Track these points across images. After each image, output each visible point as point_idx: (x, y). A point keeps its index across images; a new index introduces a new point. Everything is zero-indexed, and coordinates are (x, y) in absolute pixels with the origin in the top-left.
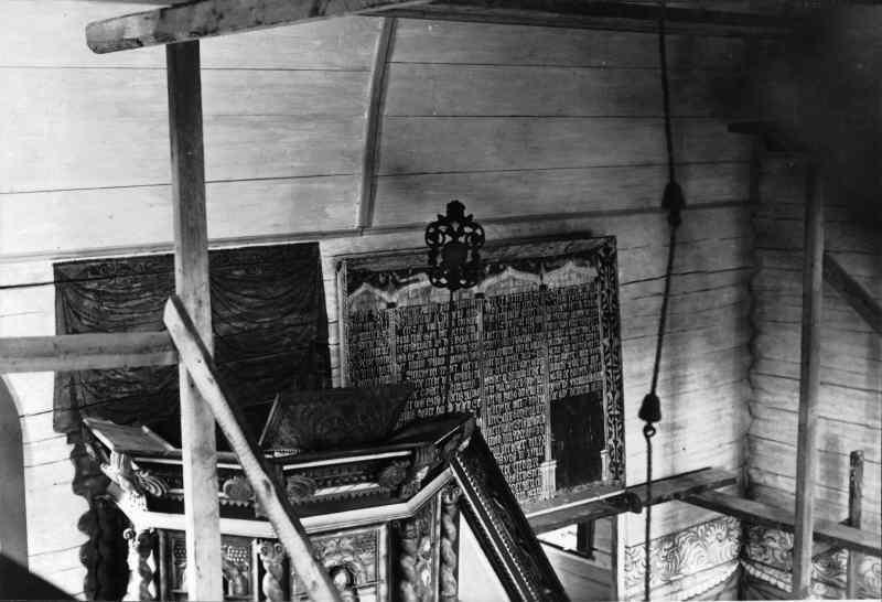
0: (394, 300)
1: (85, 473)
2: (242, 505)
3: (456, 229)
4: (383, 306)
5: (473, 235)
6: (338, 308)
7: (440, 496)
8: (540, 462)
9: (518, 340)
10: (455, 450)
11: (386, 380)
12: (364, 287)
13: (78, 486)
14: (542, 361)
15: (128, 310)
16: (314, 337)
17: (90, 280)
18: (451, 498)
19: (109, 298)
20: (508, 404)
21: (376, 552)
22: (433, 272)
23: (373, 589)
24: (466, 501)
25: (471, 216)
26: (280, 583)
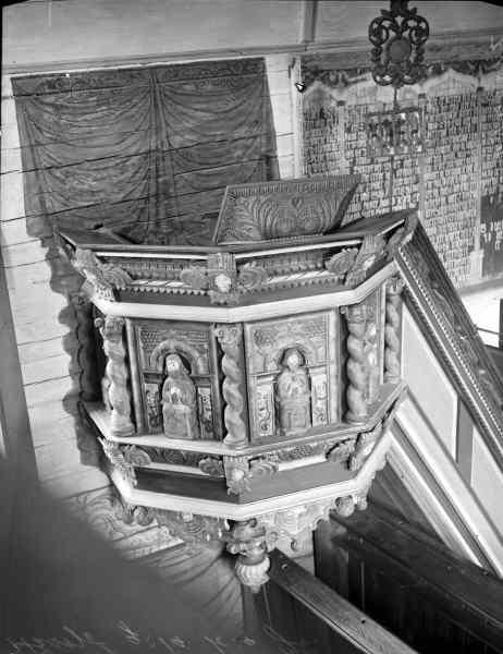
0: (343, 99)
1: (60, 273)
2: (199, 294)
3: (400, 23)
4: (333, 104)
5: (418, 29)
6: (292, 105)
7: (384, 287)
8: (469, 251)
9: (456, 139)
10: (399, 243)
11: (335, 173)
12: (316, 85)
13: (55, 284)
14: (475, 159)
15: (85, 124)
16: (263, 149)
17: (46, 94)
18: (395, 288)
19: (66, 111)
20: (443, 199)
21: (326, 336)
22: (379, 71)
23: (324, 368)
24: (408, 292)
25: (415, 9)
26: (238, 364)
